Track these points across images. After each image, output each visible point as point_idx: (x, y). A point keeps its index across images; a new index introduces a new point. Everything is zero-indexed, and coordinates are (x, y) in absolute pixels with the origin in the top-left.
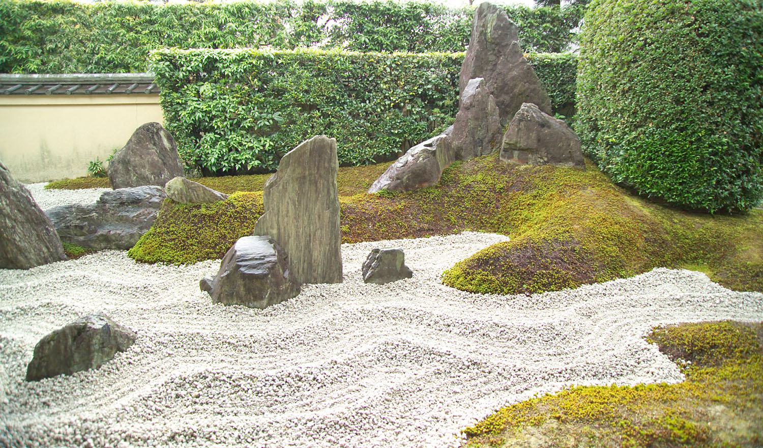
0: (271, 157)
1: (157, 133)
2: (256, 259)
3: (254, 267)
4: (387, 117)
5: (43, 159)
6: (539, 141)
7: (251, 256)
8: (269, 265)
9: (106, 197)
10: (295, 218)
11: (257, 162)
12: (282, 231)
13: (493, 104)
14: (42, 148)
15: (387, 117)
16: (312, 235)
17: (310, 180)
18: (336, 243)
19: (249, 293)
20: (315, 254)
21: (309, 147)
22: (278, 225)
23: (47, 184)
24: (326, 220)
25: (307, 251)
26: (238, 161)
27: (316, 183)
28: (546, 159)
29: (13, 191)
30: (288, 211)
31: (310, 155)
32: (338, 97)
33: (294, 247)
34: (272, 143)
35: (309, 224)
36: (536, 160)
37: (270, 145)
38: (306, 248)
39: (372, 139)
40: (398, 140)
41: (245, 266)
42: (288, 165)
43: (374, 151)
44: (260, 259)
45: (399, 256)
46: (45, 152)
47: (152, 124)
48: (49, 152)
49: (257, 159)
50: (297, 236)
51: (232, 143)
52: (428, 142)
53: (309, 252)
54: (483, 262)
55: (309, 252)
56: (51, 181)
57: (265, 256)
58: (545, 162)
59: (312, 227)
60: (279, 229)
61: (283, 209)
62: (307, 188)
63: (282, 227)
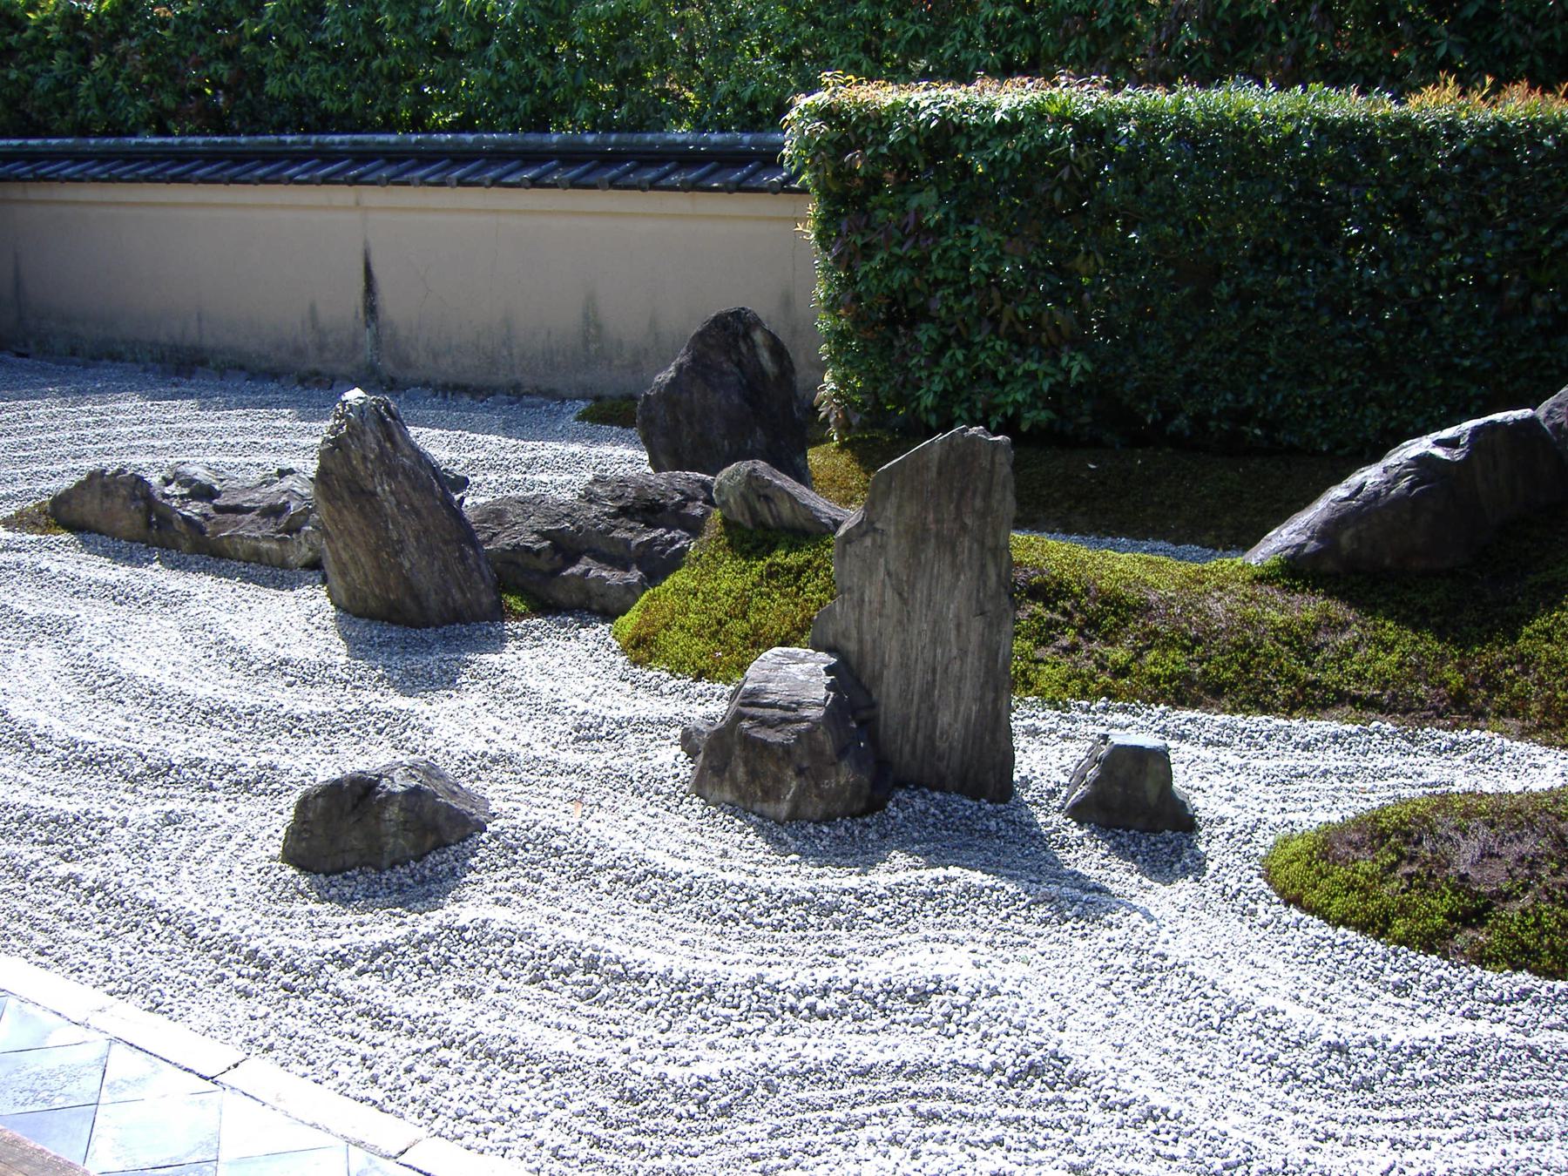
0: (1086, 406)
1: (747, 335)
2: (781, 707)
5: (586, 342)
7: (771, 698)
8: (804, 726)
9: (598, 490)
10: (900, 622)
11: (1044, 415)
14: (586, 316)
20: (944, 718)
21: (935, 456)
23: (582, 405)
24: (974, 638)
26: (996, 407)
29: (403, 466)
30: (883, 603)
31: (939, 473)
32: (1286, 247)
33: (895, 693)
34: (1088, 367)
35: (934, 642)
37: (1083, 371)
40: (1473, 391)
41: (752, 718)
43: (1391, 418)
44: (787, 709)
45: (1154, 766)
46: (592, 325)
47: (738, 315)
48: (599, 327)
51: (982, 356)
52: (1448, 433)
54: (1398, 837)
56: (598, 399)
57: (799, 704)
59: (939, 651)
60: (861, 641)
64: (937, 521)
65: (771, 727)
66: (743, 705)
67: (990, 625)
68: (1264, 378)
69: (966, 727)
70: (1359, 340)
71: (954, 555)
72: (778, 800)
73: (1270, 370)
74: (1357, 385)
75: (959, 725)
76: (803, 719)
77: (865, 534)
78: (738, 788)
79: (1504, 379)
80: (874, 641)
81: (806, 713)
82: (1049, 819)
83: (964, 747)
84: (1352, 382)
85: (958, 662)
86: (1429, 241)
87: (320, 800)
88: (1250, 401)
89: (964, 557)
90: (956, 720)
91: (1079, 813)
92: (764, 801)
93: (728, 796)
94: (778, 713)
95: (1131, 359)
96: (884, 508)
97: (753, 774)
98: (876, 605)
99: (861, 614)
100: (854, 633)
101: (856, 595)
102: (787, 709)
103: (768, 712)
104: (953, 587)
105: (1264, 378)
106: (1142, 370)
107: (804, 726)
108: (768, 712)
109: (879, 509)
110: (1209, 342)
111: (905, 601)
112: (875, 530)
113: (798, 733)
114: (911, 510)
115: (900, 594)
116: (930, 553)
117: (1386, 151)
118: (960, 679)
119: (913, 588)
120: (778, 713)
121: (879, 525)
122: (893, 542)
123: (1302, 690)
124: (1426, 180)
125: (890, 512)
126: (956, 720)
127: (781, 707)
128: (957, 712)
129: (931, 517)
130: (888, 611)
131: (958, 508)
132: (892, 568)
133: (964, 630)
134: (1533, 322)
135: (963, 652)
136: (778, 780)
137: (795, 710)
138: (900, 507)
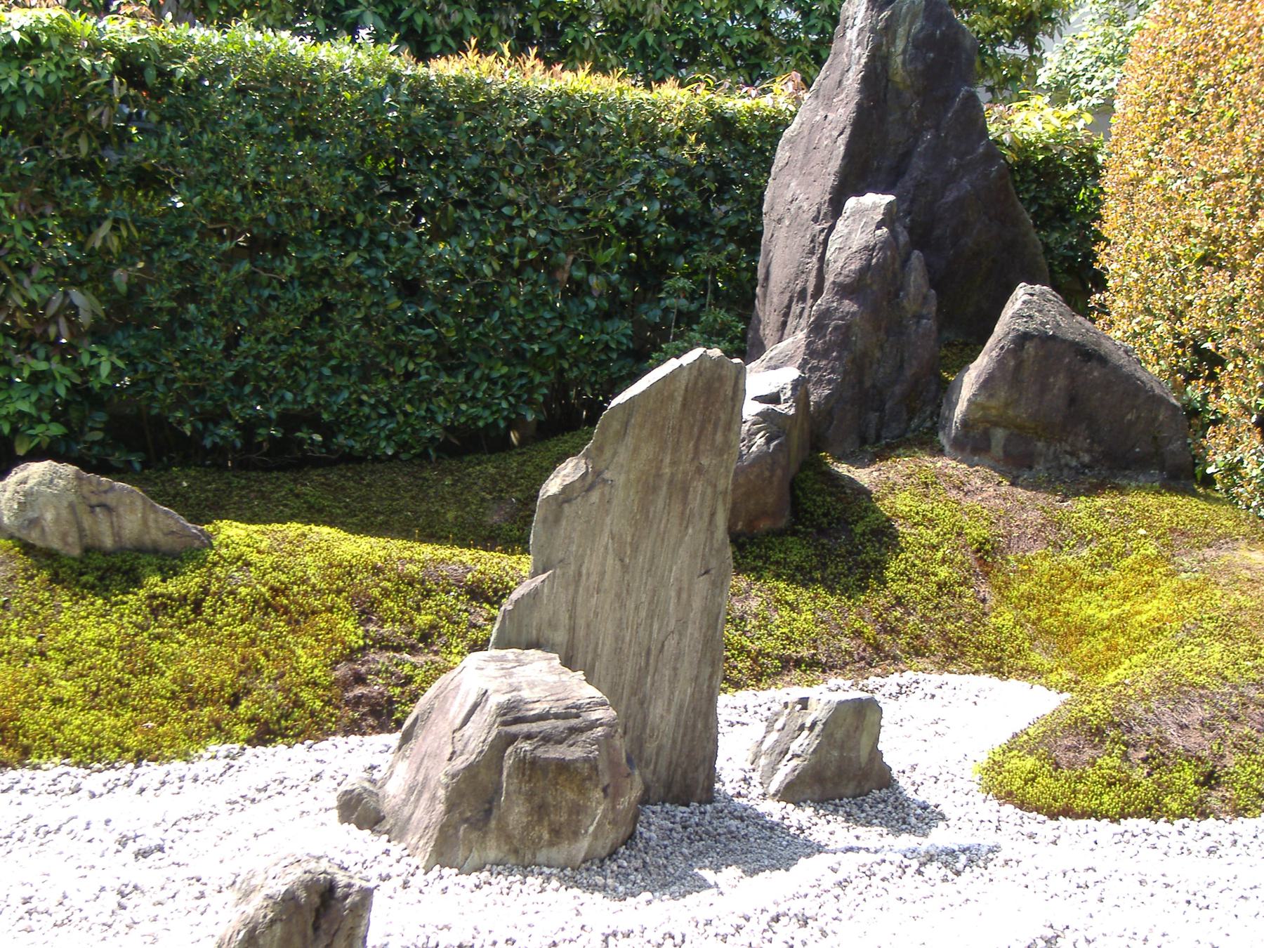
2: (557, 716)
3: (547, 739)
4: (515, 295)
6: (1072, 401)
7: (538, 708)
8: (599, 731)
10: (618, 596)
12: (581, 633)
13: (921, 281)
15: (515, 295)
16: (654, 652)
17: (671, 482)
18: (711, 677)
19: (540, 821)
20: (657, 710)
21: (682, 383)
22: (572, 617)
24: (697, 604)
25: (634, 700)
27: (685, 491)
28: (1086, 458)
31: (684, 405)
35: (651, 615)
36: (1056, 458)
38: (634, 693)
39: (451, 371)
41: (529, 737)
42: (622, 434)
44: (565, 716)
45: (871, 717)
49: (55, 418)
50: (618, 651)
53: (642, 703)
55: (642, 703)
57: (578, 707)
58: (1084, 466)
59: (656, 626)
60: (572, 630)
61: (591, 565)
62: (660, 503)
63: (581, 622)
64: (674, 463)
65: (561, 743)
66: (504, 724)
67: (714, 583)
68: (326, 371)
69: (678, 715)
70: (430, 326)
71: (685, 502)
72: (576, 835)
73: (333, 362)
74: (424, 377)
75: (672, 717)
76: (593, 725)
77: (591, 488)
78: (509, 838)
79: (566, 366)
80: (588, 626)
81: (595, 715)
82: (773, 809)
83: (674, 742)
84: (419, 375)
85: (676, 636)
86: (499, 215)
87: (278, 928)
88: (311, 401)
89: (695, 503)
90: (668, 710)
91: (791, 793)
92: (551, 844)
93: (492, 854)
94: (562, 724)
95: (168, 356)
96: (615, 454)
97: (540, 811)
98: (594, 578)
99: (576, 591)
100: (564, 618)
101: (572, 569)
102: (565, 716)
103: (546, 725)
104: (680, 542)
105: (326, 371)
106: (183, 368)
107: (599, 731)
108: (546, 725)
109: (608, 453)
110: (265, 333)
111: (625, 568)
112: (605, 481)
113: (597, 741)
114: (647, 451)
115: (622, 560)
116: (660, 503)
117: (461, 117)
118: (678, 656)
119: (635, 549)
120: (562, 724)
121: (607, 475)
122: (621, 494)
123: (755, 661)
124: (499, 150)
125: (623, 455)
126: (668, 710)
127: (557, 716)
128: (670, 701)
129: (667, 460)
130: (606, 584)
131: (696, 447)
132: (615, 530)
133: (684, 596)
134: (592, 304)
135: (683, 623)
136: (577, 810)
137: (577, 716)
138: (636, 450)
